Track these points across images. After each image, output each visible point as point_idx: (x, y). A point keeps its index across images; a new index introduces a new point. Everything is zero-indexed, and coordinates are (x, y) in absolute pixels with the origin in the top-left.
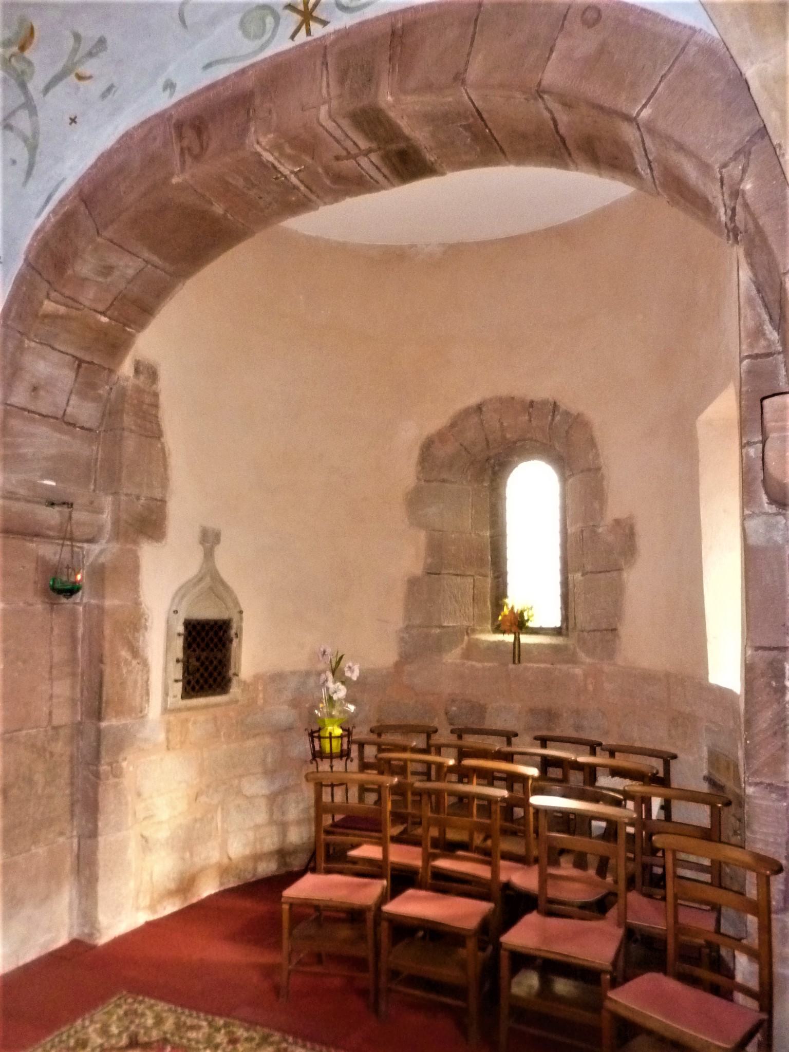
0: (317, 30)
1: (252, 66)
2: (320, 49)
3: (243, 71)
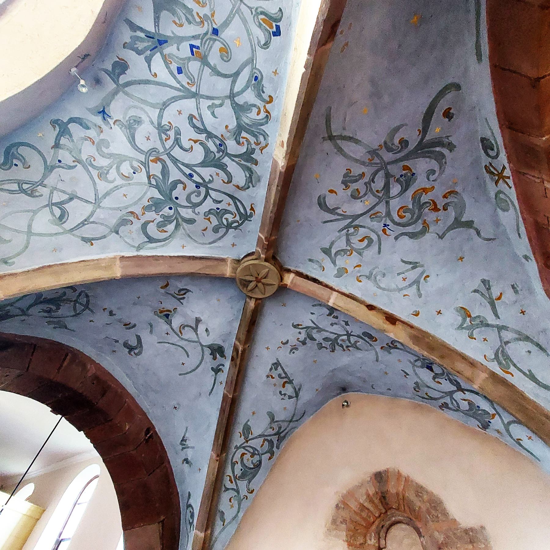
0: (507, 172)
1: (522, 213)
2: (516, 173)
3: (524, 219)
